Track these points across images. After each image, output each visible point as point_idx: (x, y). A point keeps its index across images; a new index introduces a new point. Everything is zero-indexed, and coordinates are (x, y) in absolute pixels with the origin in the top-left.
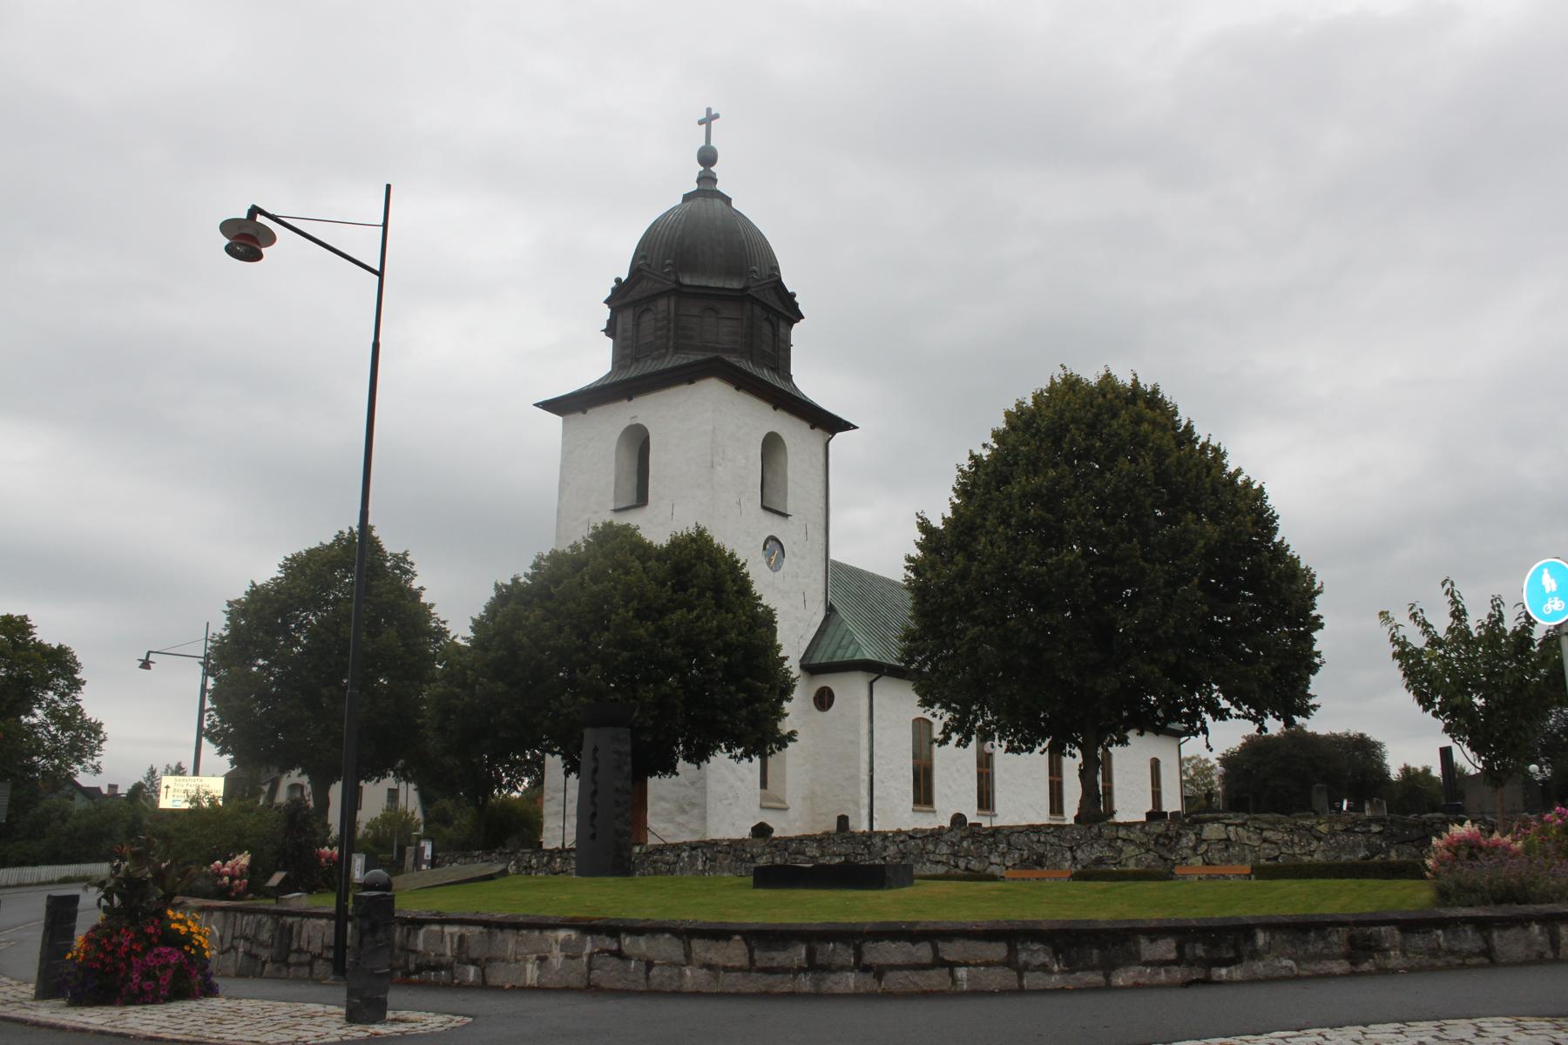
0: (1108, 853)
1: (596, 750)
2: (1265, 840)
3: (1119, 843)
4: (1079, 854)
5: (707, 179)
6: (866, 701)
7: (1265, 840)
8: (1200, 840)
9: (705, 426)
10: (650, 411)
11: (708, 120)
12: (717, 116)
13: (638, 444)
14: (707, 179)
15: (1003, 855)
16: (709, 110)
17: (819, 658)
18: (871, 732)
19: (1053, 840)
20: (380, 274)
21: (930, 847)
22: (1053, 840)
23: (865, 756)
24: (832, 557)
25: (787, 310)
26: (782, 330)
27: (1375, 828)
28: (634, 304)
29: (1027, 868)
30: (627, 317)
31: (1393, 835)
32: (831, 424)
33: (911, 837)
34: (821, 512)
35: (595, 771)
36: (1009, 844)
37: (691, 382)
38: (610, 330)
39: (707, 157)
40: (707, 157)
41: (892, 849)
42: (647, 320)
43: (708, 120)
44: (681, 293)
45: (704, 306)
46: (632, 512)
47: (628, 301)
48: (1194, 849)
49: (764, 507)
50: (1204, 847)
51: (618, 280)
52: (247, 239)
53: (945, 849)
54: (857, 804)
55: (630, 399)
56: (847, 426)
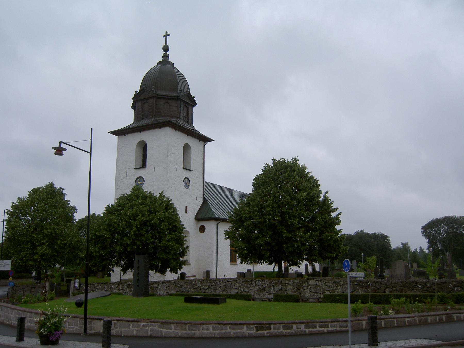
0: (283, 287)
1: (139, 261)
2: (326, 285)
3: (287, 285)
4: (275, 287)
5: (166, 56)
6: (216, 230)
7: (326, 285)
8: (309, 285)
9: (165, 143)
10: (148, 137)
11: (166, 35)
12: (169, 35)
13: (143, 147)
14: (166, 56)
15: (254, 287)
16: (166, 32)
17: (201, 216)
18: (217, 240)
19: (268, 283)
20: (91, 153)
21: (233, 284)
22: (268, 283)
23: (215, 247)
24: (205, 180)
25: (191, 102)
26: (190, 109)
27: (356, 283)
28: (142, 100)
29: (261, 292)
30: (139, 104)
31: (360, 285)
32: (205, 140)
33: (228, 281)
34: (202, 169)
35: (138, 267)
36: (256, 284)
37: (161, 128)
38: (133, 107)
39: (166, 49)
40: (166, 49)
41: (222, 285)
42: (146, 105)
43: (166, 35)
44: (158, 97)
45: (164, 102)
46: (141, 169)
47: (140, 100)
48: (307, 287)
49: (184, 168)
50: (310, 287)
51: (136, 92)
52: (59, 151)
53: (237, 285)
54: (212, 263)
55: (140, 132)
56: (211, 140)
